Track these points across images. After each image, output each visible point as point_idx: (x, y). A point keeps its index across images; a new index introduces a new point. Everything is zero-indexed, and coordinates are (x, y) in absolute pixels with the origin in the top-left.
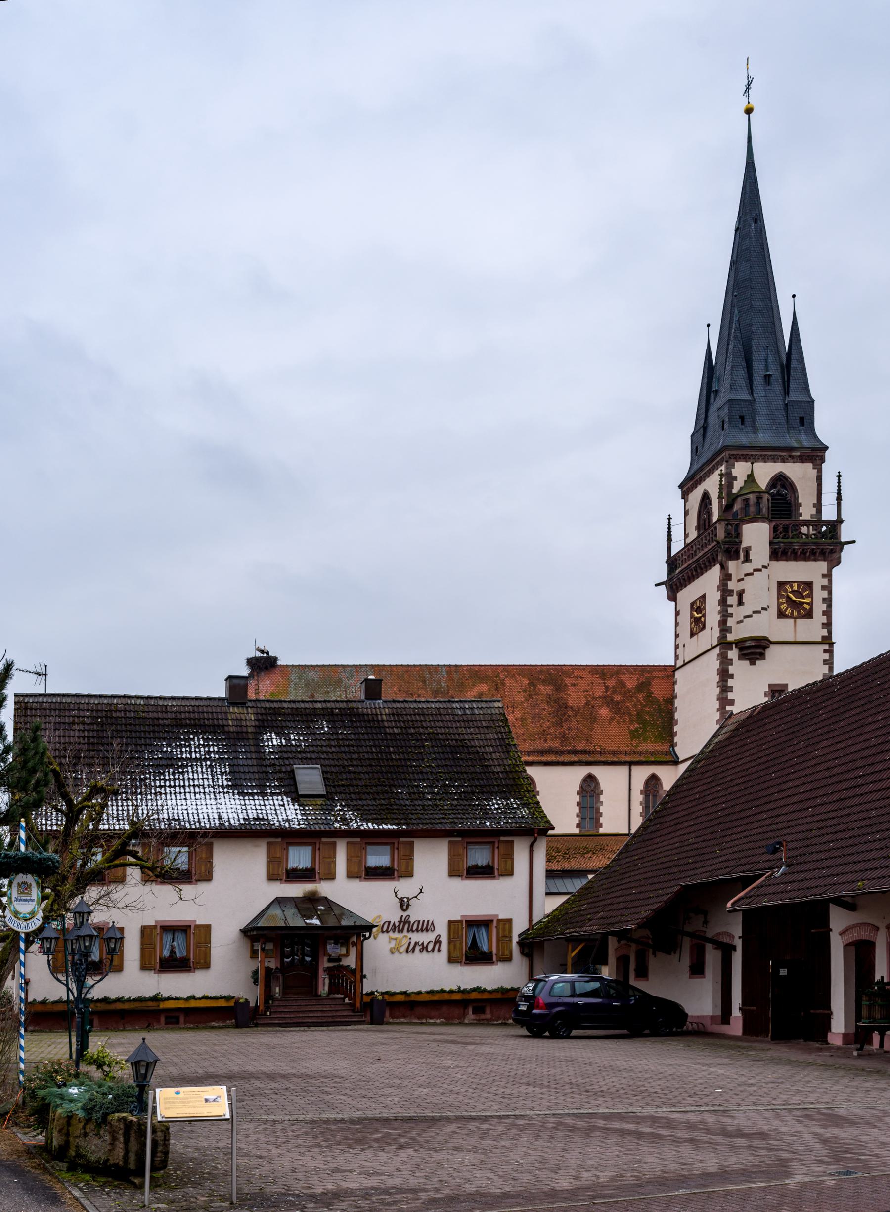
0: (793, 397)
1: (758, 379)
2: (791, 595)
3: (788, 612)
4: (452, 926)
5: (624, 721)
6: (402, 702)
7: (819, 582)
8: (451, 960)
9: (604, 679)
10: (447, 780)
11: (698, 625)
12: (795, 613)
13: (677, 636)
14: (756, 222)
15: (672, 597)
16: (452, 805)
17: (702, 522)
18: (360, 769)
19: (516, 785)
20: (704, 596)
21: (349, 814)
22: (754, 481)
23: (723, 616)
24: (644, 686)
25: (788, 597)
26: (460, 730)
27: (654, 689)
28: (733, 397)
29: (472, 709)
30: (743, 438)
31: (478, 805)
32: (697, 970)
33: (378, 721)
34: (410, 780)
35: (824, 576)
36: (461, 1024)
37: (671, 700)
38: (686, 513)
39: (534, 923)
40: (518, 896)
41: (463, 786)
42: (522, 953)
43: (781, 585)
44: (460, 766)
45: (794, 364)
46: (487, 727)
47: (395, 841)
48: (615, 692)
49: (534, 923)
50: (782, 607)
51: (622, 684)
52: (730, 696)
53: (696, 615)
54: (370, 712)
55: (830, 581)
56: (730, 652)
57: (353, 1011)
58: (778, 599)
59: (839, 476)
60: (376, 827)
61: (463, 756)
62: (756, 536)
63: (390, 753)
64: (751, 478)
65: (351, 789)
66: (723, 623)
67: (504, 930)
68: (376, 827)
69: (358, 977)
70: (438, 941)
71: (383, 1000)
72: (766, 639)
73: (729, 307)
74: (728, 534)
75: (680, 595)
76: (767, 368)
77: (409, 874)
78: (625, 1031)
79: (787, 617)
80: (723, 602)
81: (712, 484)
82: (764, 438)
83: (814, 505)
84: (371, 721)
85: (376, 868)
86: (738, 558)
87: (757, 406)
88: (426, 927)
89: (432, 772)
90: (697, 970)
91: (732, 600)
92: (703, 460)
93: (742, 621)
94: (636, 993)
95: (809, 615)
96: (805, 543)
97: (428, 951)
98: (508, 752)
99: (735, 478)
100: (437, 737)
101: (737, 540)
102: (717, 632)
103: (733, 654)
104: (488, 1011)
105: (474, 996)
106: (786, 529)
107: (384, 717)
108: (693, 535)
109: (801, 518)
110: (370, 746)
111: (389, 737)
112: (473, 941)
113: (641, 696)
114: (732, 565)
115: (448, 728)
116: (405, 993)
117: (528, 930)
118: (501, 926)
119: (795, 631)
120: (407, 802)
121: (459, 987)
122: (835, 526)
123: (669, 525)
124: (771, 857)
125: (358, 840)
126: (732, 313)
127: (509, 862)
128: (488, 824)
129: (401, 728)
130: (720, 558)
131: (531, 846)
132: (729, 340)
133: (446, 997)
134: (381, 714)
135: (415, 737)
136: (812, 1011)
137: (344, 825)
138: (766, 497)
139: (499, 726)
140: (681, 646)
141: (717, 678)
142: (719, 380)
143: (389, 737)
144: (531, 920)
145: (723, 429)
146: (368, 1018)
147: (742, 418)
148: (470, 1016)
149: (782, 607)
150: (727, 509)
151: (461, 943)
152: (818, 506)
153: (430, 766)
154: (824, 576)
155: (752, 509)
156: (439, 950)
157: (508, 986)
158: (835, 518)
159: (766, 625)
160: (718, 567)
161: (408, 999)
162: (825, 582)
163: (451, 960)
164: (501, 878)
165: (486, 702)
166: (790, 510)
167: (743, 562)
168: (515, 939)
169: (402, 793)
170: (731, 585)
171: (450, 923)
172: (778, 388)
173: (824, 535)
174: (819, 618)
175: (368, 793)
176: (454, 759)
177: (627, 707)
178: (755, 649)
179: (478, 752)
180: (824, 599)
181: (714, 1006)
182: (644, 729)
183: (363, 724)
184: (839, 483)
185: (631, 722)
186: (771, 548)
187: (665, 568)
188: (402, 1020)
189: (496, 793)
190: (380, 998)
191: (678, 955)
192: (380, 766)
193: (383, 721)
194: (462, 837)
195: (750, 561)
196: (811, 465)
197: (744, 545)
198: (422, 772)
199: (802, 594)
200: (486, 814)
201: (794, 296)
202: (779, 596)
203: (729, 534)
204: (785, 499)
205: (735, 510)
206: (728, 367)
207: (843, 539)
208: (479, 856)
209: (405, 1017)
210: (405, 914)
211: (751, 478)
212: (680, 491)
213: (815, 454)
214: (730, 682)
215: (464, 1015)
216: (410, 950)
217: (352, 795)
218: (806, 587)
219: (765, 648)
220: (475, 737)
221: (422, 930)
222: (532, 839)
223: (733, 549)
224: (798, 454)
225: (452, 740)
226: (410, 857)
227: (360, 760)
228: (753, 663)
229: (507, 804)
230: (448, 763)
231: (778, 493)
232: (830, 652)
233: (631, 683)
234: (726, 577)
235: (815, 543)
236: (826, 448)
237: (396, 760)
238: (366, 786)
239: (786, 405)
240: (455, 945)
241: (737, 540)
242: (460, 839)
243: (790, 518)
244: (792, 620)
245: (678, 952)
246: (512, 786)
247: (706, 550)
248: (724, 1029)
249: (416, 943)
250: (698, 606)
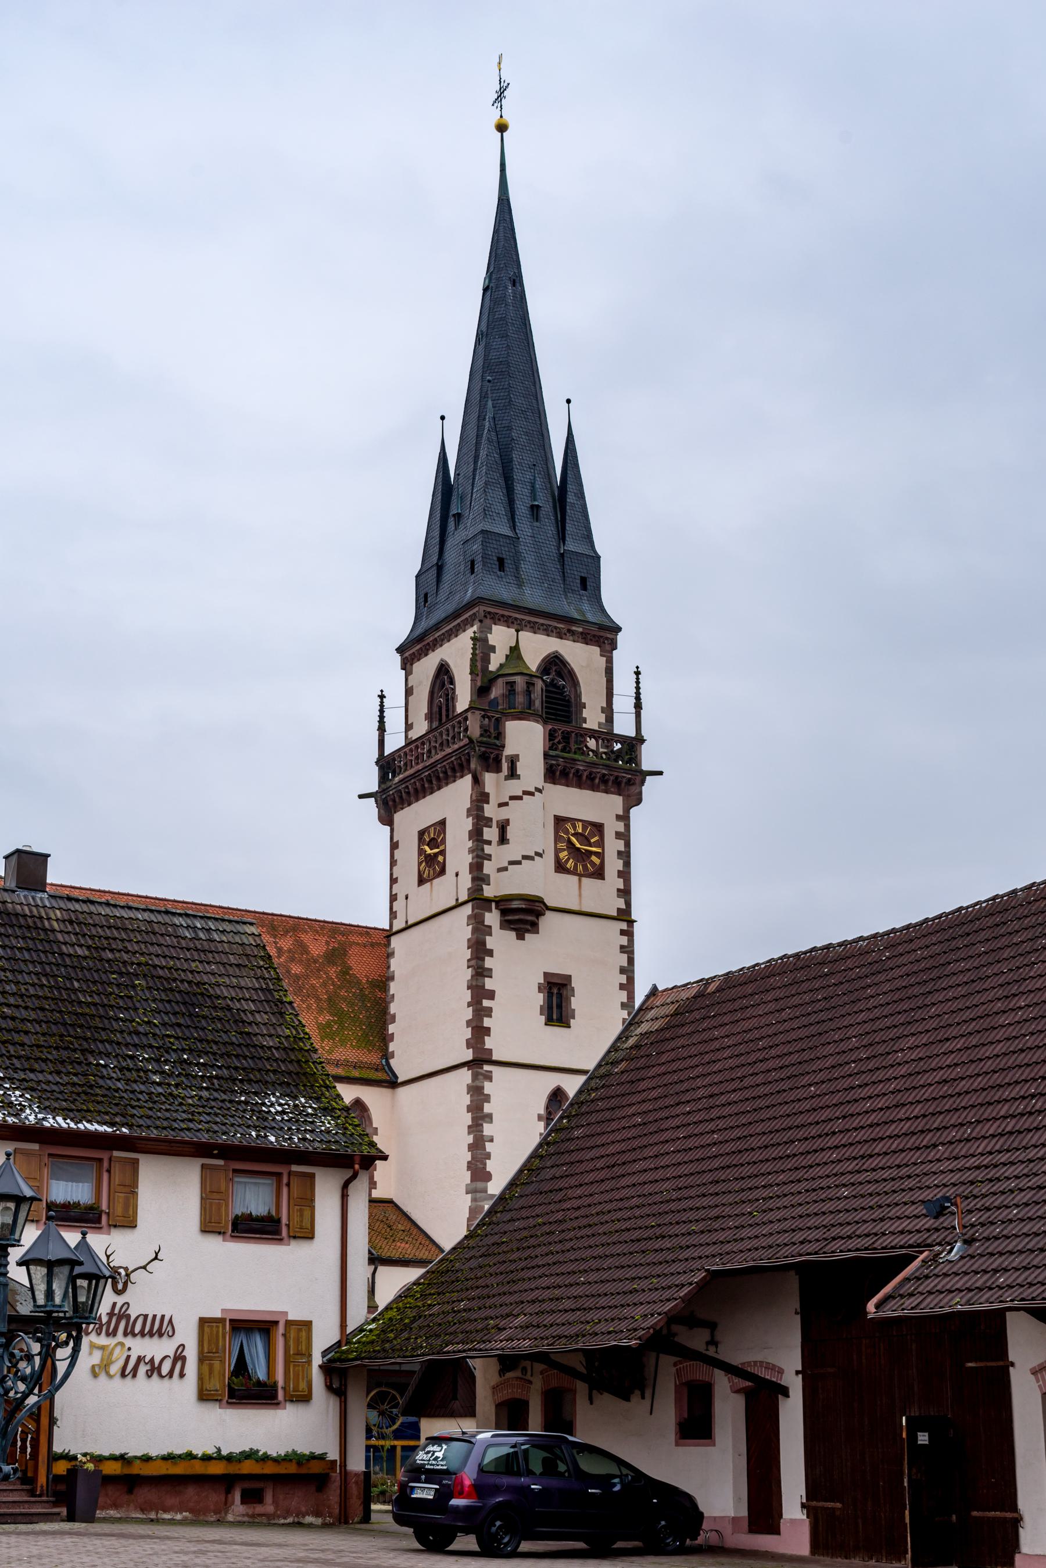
0: (571, 545)
1: (522, 508)
2: (573, 839)
3: (570, 865)
4: (207, 1329)
5: (309, 1007)
6: (84, 902)
7: (612, 826)
8: (204, 1396)
9: (275, 937)
10: (183, 1050)
11: (432, 866)
12: (580, 868)
13: (393, 881)
14: (514, 285)
15: (387, 818)
16: (201, 1097)
17: (435, 709)
18: (24, 1014)
19: (305, 1074)
20: (443, 823)
21: (15, 1096)
22: (520, 657)
23: (478, 856)
24: (336, 956)
25: (569, 842)
26: (193, 965)
27: (352, 962)
28: (488, 527)
29: (209, 930)
30: (503, 590)
31: (246, 1103)
32: (696, 1427)
33: (45, 930)
34: (118, 1044)
35: (619, 818)
36: (220, 1522)
37: (383, 982)
38: (409, 692)
39: (349, 1330)
40: (312, 1282)
41: (213, 1066)
42: (329, 1388)
43: (560, 821)
44: (203, 1029)
45: (571, 498)
46: (238, 966)
47: (104, 1155)
48: (292, 959)
49: (349, 1330)
51: (303, 948)
52: (489, 984)
53: (429, 851)
54: (27, 912)
55: (627, 827)
56: (487, 915)
57: (32, 1493)
58: (556, 844)
59: (638, 673)
60: (72, 1125)
61: (206, 1012)
62: (526, 739)
63: (75, 991)
64: (515, 652)
65: (11, 1048)
66: (476, 868)
67: (298, 1341)
68: (72, 1125)
69: (44, 1421)
70: (179, 1358)
71: (97, 1472)
72: (540, 900)
73: (477, 396)
74: (485, 731)
75: (398, 817)
76: (533, 495)
77: (129, 1223)
78: (580, 1545)
80: (476, 834)
81: (457, 652)
82: (533, 596)
83: (603, 710)
84: (32, 927)
85: (66, 1206)
86: (498, 770)
87: (522, 548)
88: (158, 1328)
89: (154, 1035)
90: (696, 1427)
91: (491, 833)
92: (439, 614)
93: (505, 869)
94: (625, 1471)
95: (599, 873)
96: (593, 764)
97: (161, 1376)
98: (281, 1014)
99: (493, 649)
100: (154, 973)
101: (497, 742)
102: (466, 881)
103: (492, 918)
104: (269, 1497)
105: (248, 1467)
106: (566, 737)
107: (55, 924)
108: (421, 728)
109: (584, 725)
110: (37, 974)
111: (68, 961)
112: (241, 1361)
113: (333, 971)
114: (490, 780)
115: (172, 958)
116: (122, 1458)
117: (339, 1344)
118: (292, 1334)
119: (580, 895)
120: (119, 1085)
121: (219, 1450)
122: (633, 744)
123: (382, 705)
124: (930, 1223)
125: (36, 1147)
126: (482, 407)
127: (307, 1213)
128: (272, 1139)
129: (89, 947)
130: (473, 766)
131: (345, 1186)
132: (478, 444)
133: (199, 1468)
134: (49, 919)
135: (115, 968)
136: (975, 1513)
137: (10, 1115)
138: (539, 684)
139: (260, 967)
140: (401, 898)
141: (468, 954)
142: (462, 498)
143: (68, 961)
144: (343, 1325)
145: (472, 572)
146: (64, 1511)
147: (501, 562)
148: (238, 1508)
150: (481, 691)
151: (222, 1362)
152: (608, 711)
153: (149, 1023)
154: (619, 818)
155: (520, 699)
156: (182, 1375)
157: (304, 1449)
158: (633, 734)
159: (538, 879)
160: (468, 778)
161: (127, 1471)
162: (620, 827)
163: (204, 1396)
164: (293, 1243)
165: (230, 921)
166: (569, 712)
167: (507, 778)
168: (317, 1360)
169: (105, 1066)
170: (489, 810)
171: (203, 1322)
172: (549, 527)
173: (618, 755)
174: (613, 880)
175: (45, 1061)
176: (190, 1015)
177: (313, 987)
178: (524, 915)
179: (230, 1009)
180: (619, 853)
181: (737, 1500)
182: (342, 1027)
183: (19, 932)
184: (638, 682)
185: (320, 1011)
186: (546, 763)
187: (374, 772)
188: (112, 1513)
189: (273, 1083)
190: (90, 1466)
191: (647, 1402)
192: (60, 1012)
193: (53, 931)
194: (229, 1159)
195: (518, 777)
196: (597, 649)
197: (508, 751)
198: (137, 1033)
199: (589, 841)
200: (264, 1121)
201: (568, 401)
202: (557, 839)
203: (486, 731)
204: (562, 694)
205: (492, 696)
206: (479, 483)
207: (645, 766)
208: (254, 1198)
209: (115, 1506)
210: (120, 1300)
211: (515, 652)
212: (398, 658)
213: (604, 635)
214: (488, 962)
215: (227, 1505)
216: (128, 1372)
217: (15, 1061)
218: (594, 830)
219: (539, 914)
220: (221, 980)
221: (151, 1334)
222: (349, 1173)
223: (490, 756)
224: (581, 630)
225: (182, 981)
226: (131, 1190)
227: (22, 996)
228: (521, 937)
229: (296, 1106)
230: (181, 1021)
231: (552, 684)
232: (628, 933)
233: (317, 948)
234: (481, 798)
235: (607, 766)
236: (619, 629)
237: (88, 1004)
238: (38, 1046)
239: (562, 555)
240: (211, 1367)
241: (497, 742)
242: (221, 1162)
243: (570, 722)
244: (576, 878)
245: (648, 1393)
246: (297, 1074)
247: (449, 750)
248: (765, 1542)
249: (140, 1359)
250: (433, 838)
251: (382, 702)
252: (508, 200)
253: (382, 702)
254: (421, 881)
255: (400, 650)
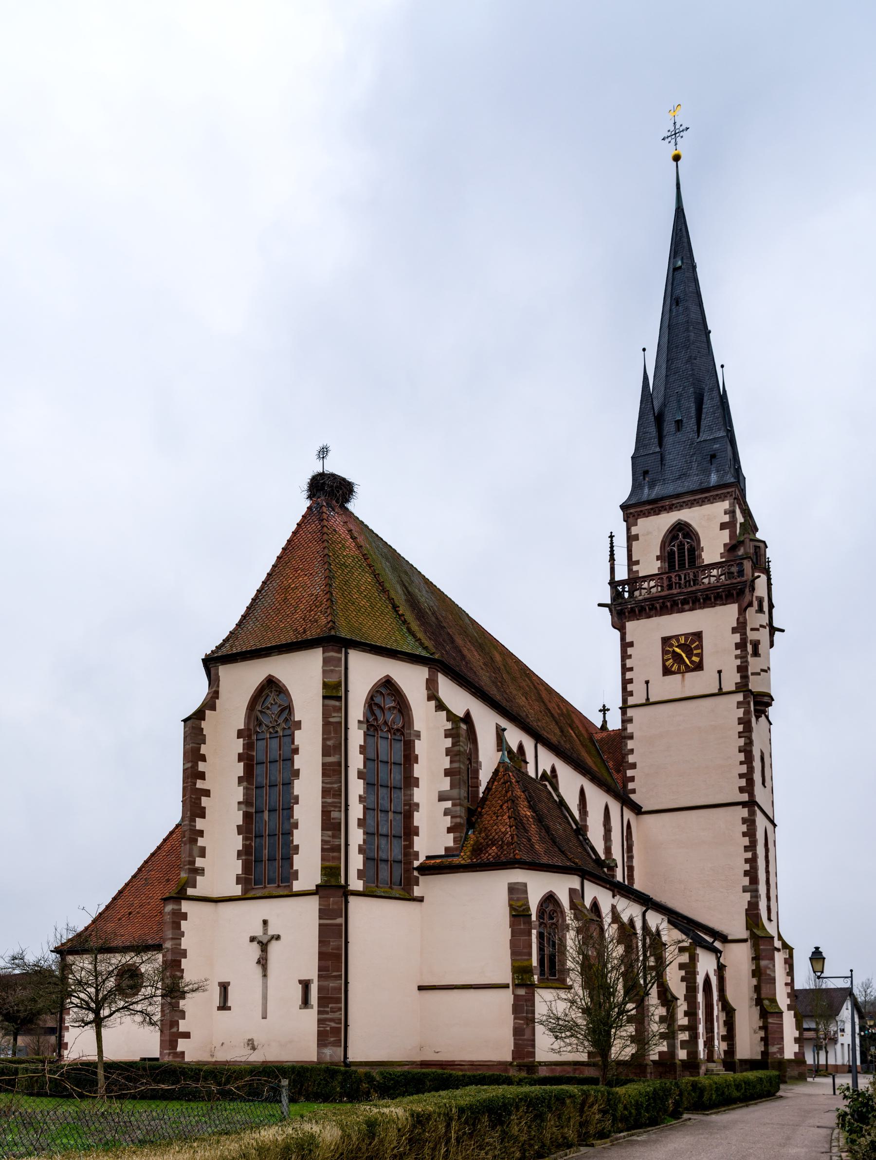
15: (619, 625)
43: (666, 641)
50: (667, 663)
52: (202, 766)
79: (674, 673)
123: (612, 543)
149: (667, 663)
201: (644, 350)
202: (664, 652)
251: (612, 541)
252: (683, 210)
253: (612, 541)
254: (667, 671)
255: (623, 507)
